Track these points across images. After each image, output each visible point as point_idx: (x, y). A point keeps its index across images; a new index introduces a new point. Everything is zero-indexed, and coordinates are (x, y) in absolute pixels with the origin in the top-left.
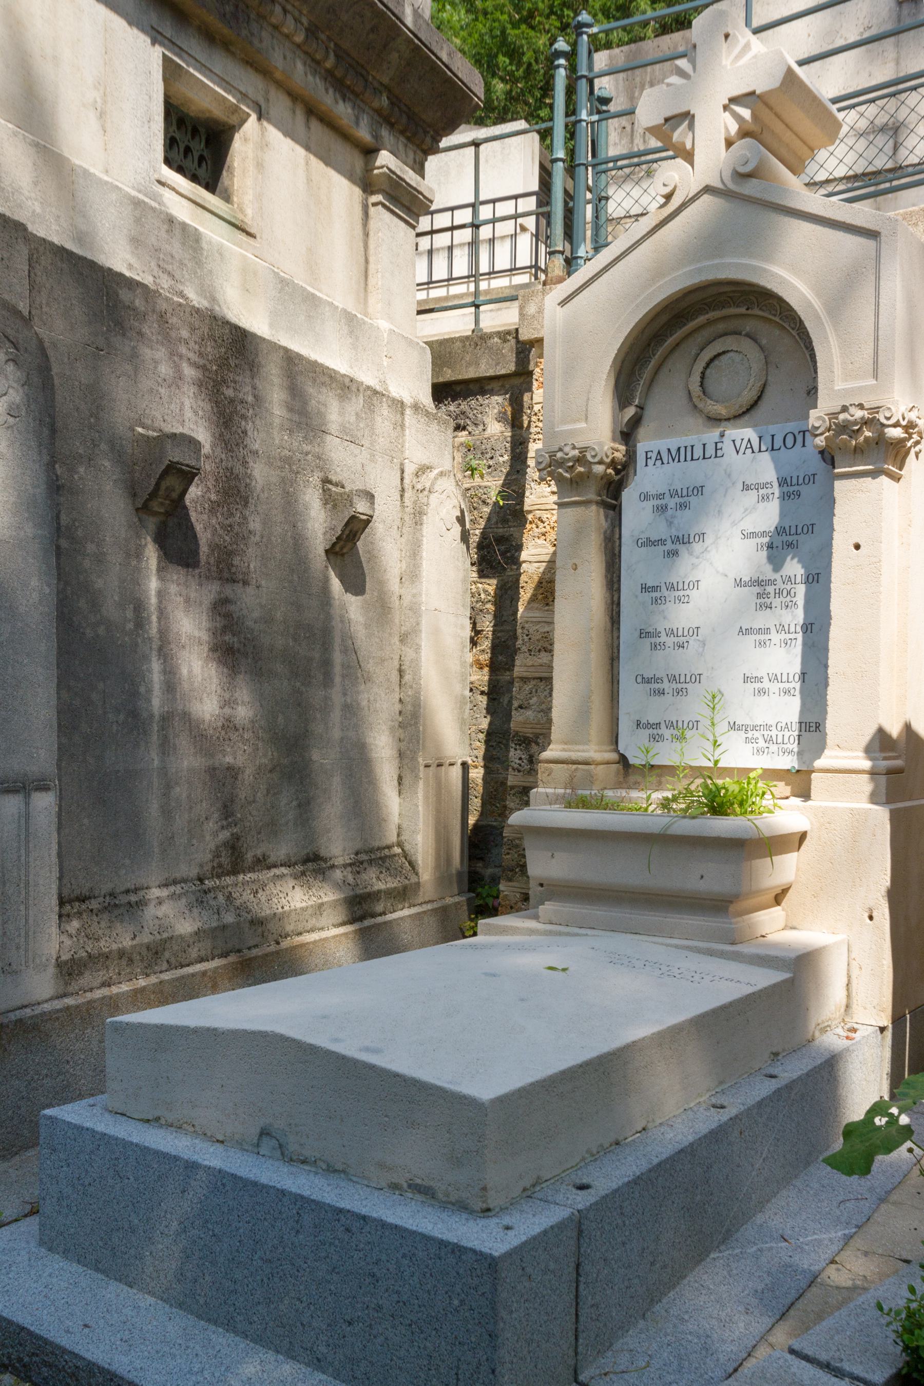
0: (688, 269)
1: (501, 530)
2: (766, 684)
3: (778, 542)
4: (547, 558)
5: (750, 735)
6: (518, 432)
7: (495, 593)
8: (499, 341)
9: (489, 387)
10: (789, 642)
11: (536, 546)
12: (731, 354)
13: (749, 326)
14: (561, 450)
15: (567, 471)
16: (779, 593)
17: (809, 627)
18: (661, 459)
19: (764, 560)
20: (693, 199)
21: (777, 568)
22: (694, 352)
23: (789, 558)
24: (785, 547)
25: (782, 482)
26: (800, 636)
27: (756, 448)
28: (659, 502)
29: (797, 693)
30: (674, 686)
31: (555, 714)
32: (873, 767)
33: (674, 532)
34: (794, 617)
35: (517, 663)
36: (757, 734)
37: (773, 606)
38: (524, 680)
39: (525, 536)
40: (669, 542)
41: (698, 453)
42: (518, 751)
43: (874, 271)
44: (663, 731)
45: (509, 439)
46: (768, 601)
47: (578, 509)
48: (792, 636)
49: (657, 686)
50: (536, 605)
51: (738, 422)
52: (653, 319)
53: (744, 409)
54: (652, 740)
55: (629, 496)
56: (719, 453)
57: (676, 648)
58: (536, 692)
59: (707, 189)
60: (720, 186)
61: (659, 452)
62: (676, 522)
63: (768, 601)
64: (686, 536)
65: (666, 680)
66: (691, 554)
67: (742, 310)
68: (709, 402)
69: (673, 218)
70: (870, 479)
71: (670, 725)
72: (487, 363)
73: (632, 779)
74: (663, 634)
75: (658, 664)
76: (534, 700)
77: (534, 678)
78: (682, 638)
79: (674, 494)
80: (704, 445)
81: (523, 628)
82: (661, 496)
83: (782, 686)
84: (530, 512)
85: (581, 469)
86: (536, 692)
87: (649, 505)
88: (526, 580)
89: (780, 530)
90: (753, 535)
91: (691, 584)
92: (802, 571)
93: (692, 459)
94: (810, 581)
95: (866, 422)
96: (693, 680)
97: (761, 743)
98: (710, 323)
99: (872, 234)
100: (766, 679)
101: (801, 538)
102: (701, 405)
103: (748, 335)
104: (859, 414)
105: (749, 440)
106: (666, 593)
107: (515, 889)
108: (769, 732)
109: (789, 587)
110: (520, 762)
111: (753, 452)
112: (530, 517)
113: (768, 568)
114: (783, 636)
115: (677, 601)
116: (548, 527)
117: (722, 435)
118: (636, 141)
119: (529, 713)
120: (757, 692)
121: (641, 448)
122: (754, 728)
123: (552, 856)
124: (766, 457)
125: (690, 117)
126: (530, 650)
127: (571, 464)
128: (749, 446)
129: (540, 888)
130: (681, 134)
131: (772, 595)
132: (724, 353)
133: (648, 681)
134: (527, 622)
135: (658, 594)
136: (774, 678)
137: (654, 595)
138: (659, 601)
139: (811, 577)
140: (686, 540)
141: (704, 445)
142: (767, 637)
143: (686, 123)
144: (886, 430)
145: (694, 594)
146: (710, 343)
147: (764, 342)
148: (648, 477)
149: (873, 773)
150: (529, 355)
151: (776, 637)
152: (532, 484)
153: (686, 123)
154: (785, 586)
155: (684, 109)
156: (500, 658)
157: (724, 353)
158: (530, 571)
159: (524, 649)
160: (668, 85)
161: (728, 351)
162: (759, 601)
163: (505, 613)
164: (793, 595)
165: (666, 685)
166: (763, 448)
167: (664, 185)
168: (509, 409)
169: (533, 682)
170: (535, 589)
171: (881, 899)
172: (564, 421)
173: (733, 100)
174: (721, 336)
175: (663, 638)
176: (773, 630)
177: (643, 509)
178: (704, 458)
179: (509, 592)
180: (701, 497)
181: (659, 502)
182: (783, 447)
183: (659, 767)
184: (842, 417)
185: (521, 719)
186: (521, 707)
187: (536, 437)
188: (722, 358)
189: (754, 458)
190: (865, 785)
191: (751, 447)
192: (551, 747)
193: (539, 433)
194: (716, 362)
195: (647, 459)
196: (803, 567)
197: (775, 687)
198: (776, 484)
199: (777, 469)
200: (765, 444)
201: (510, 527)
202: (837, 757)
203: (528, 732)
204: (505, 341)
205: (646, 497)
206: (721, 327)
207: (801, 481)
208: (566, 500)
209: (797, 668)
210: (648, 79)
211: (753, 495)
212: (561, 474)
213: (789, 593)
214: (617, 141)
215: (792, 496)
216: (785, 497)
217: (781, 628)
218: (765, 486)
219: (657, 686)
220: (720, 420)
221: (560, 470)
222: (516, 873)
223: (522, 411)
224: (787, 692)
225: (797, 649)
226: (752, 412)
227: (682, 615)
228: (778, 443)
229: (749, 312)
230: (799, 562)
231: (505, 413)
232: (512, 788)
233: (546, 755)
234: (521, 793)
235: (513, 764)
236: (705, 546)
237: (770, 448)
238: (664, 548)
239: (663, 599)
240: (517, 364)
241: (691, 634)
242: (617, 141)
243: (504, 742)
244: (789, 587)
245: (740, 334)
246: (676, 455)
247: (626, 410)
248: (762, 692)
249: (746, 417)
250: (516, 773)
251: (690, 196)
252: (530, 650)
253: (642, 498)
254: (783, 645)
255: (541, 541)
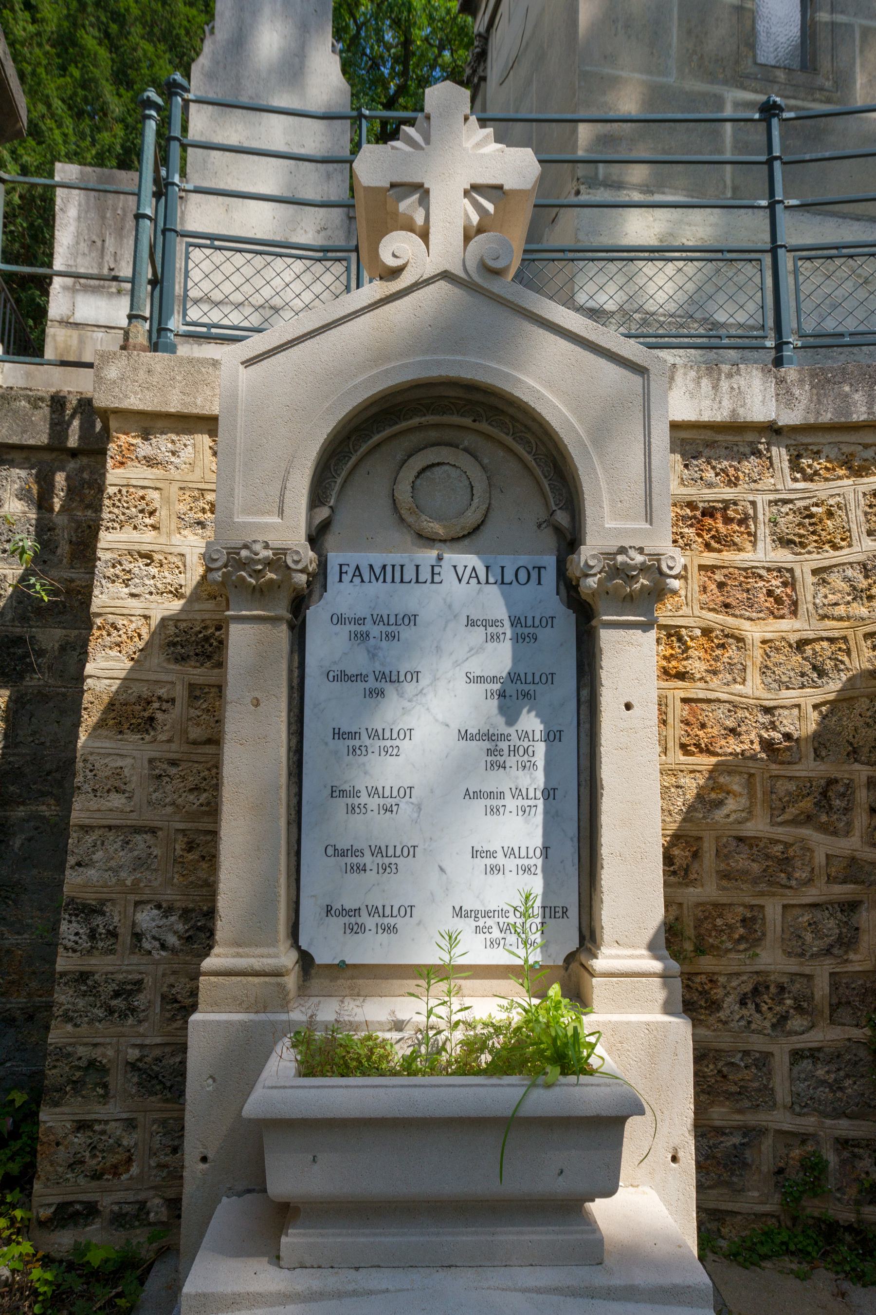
0: (418, 359)
1: (18, 630)
2: (500, 860)
3: (511, 690)
4: (123, 674)
5: (481, 923)
6: (47, 515)
7: (7, 706)
8: (27, 405)
9: (9, 457)
10: (528, 809)
11: (108, 658)
12: (446, 468)
13: (468, 440)
14: (246, 547)
15: (251, 576)
16: (516, 750)
17: (552, 792)
18: (360, 575)
19: (495, 710)
20: (428, 282)
21: (511, 720)
22: (399, 457)
23: (525, 711)
24: (521, 697)
25: (515, 622)
26: (540, 803)
27: (483, 578)
28: (358, 628)
29: (539, 871)
30: (379, 860)
31: (223, 903)
32: (665, 969)
33: (378, 667)
34: (533, 780)
35: (76, 806)
36: (490, 922)
37: (507, 765)
38: (86, 829)
39: (92, 644)
40: (371, 678)
41: (410, 574)
42: (75, 925)
43: (641, 408)
44: (364, 919)
45: (34, 522)
46: (502, 759)
47: (261, 626)
48: (530, 803)
49: (355, 860)
50: (104, 732)
51: (456, 545)
52: (366, 409)
53: (466, 532)
54: (348, 931)
55: (317, 616)
56: (437, 579)
57: (382, 812)
58: (103, 844)
59: (446, 275)
60: (462, 275)
61: (357, 567)
62: (380, 654)
63: (502, 759)
64: (394, 673)
65: (367, 852)
66: (401, 695)
67: (467, 421)
68: (424, 517)
69: (401, 297)
70: (640, 631)
71: (374, 911)
72: (10, 428)
73: (316, 984)
74: (364, 793)
75: (356, 830)
76: (99, 855)
77: (100, 827)
78: (389, 800)
79: (378, 620)
80: (417, 566)
81: (85, 761)
82: (361, 621)
83: (520, 862)
84: (99, 615)
85: (270, 575)
86: (103, 844)
87: (344, 630)
88: (92, 699)
89: (513, 677)
90: (480, 679)
91: (402, 732)
92: (541, 727)
93: (402, 581)
94: (551, 738)
95: (643, 569)
96: (405, 854)
97: (496, 933)
98: (420, 427)
99: (640, 370)
100: (500, 854)
101: (540, 688)
102: (410, 519)
103: (466, 450)
104: (639, 559)
105: (474, 569)
106: (368, 742)
107: (65, 1117)
108: (505, 920)
109: (526, 744)
110: (77, 938)
111: (479, 583)
112: (99, 621)
113: (500, 721)
114: (520, 802)
115: (383, 753)
116: (124, 637)
117: (440, 558)
118: (107, 258)
119: (91, 872)
120: (489, 869)
121: (334, 559)
122: (487, 914)
123: (314, 1160)
124: (494, 591)
125: (421, 190)
126: (94, 790)
127: (260, 567)
128: (474, 575)
129: (202, 1166)
130: (409, 206)
131: (506, 752)
132: (439, 464)
133: (343, 854)
134: (92, 754)
135: (357, 743)
136: (510, 853)
137: (351, 743)
138: (358, 752)
139: (552, 734)
140: (394, 678)
141: (417, 566)
142: (501, 802)
143: (417, 196)
144: (668, 581)
145: (405, 745)
146: (420, 450)
147: (486, 461)
148: (342, 597)
149: (664, 976)
150: (67, 429)
151: (511, 803)
152: (103, 582)
153: (417, 196)
154: (521, 743)
155: (417, 180)
156: (12, 788)
157: (439, 464)
158: (97, 689)
159: (87, 787)
160: (393, 148)
161: (443, 464)
162: (489, 759)
163: (20, 732)
164: (531, 753)
165: (368, 859)
166: (491, 580)
167: (394, 256)
168: (35, 489)
169: (98, 832)
170: (104, 712)
171: (687, 1134)
172: (247, 511)
173: (475, 188)
174: (433, 445)
175: (364, 799)
176: (508, 795)
177: (336, 634)
178: (417, 582)
179: (28, 707)
180: (413, 627)
181: (358, 628)
182: (515, 582)
183: (355, 966)
184: (620, 558)
185: (79, 880)
186: (79, 864)
187: (110, 524)
188: (436, 469)
189: (480, 590)
190: (656, 991)
191: (477, 577)
192: (216, 950)
193: (114, 521)
194: (428, 473)
195: (341, 573)
196: (542, 722)
197: (511, 864)
198: (507, 623)
199: (508, 606)
200: (493, 576)
201: (31, 627)
202: (618, 957)
203: (90, 898)
204: (36, 407)
205: (339, 619)
206: (433, 435)
207: (537, 623)
208: (244, 613)
209: (537, 841)
210: (121, 205)
211: (479, 634)
212: (243, 579)
213: (526, 751)
214: (86, 252)
215: (527, 639)
216: (517, 639)
217: (517, 793)
218: (494, 623)
219: (355, 860)
220: (434, 540)
221: (243, 573)
222: (66, 1093)
223: (53, 492)
224: (527, 870)
225: (538, 818)
226: (473, 537)
227: (388, 771)
228: (509, 576)
229: (476, 426)
230: (537, 716)
231: (29, 490)
232: (63, 974)
233: (209, 963)
234: (76, 981)
235: (65, 942)
236: (420, 688)
237: (500, 581)
238: (364, 685)
239: (363, 749)
240: (51, 437)
241: (402, 795)
242: (86, 252)
243: (13, 896)
244: (526, 744)
245: (457, 447)
246: (381, 574)
247: (317, 510)
248: (495, 869)
249: (466, 542)
250: (70, 954)
251: (425, 277)
252: (94, 790)
253: (335, 621)
254: (520, 813)
255: (114, 653)
